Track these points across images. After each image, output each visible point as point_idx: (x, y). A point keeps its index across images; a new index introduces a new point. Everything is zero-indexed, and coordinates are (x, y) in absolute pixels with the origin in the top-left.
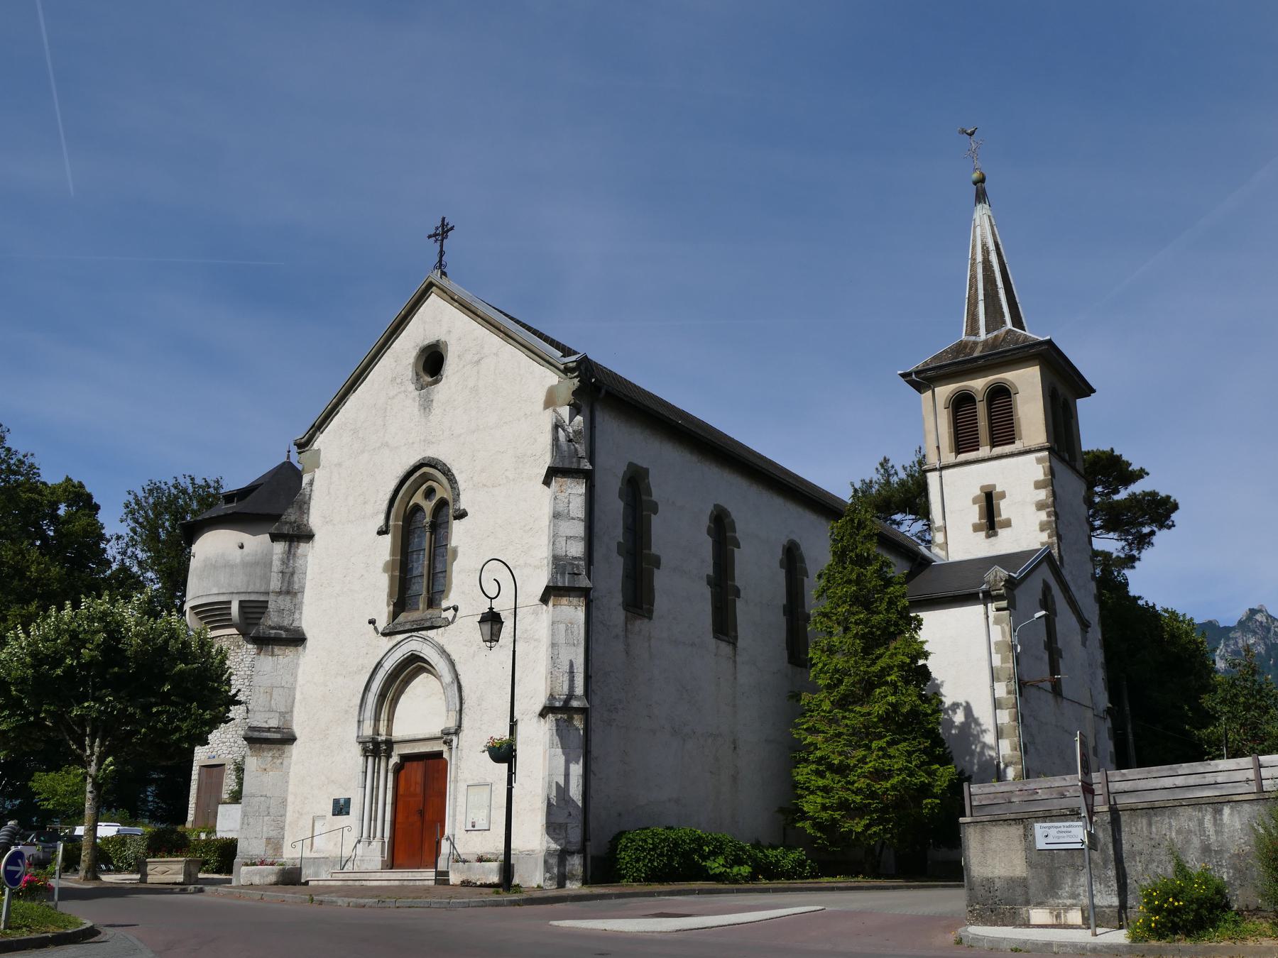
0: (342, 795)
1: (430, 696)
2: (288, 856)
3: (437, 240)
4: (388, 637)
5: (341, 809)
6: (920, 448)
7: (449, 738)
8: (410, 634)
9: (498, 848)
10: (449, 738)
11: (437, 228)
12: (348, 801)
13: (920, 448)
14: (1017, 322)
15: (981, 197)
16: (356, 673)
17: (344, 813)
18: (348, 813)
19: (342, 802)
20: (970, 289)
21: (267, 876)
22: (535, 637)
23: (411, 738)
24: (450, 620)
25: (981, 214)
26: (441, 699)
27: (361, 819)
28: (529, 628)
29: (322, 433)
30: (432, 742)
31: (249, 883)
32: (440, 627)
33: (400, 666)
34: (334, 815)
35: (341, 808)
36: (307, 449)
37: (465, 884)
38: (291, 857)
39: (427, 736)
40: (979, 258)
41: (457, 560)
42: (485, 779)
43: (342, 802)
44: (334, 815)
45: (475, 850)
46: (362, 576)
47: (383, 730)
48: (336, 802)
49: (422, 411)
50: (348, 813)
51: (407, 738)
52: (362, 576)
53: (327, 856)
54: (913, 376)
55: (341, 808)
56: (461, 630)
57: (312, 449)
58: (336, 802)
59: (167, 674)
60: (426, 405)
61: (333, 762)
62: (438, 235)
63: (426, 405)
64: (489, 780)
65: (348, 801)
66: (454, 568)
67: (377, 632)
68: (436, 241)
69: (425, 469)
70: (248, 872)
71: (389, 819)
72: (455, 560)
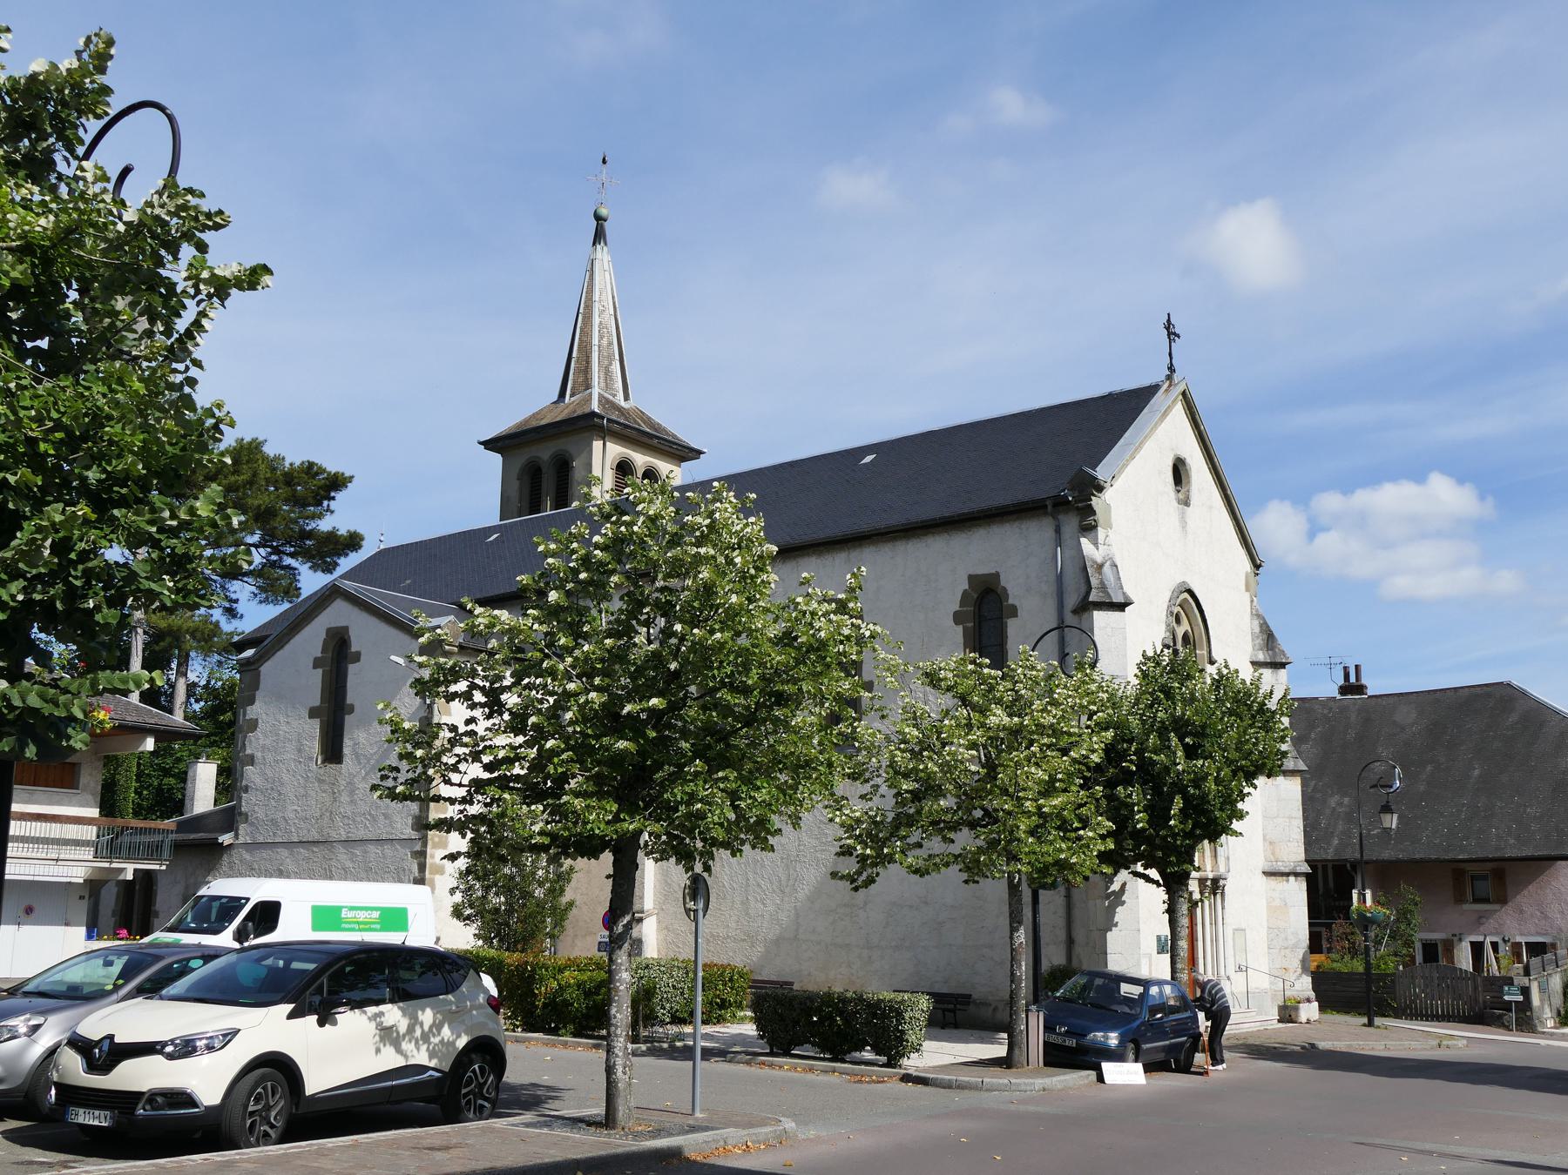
14: (626, 398)
20: (601, 338)
25: (603, 255)
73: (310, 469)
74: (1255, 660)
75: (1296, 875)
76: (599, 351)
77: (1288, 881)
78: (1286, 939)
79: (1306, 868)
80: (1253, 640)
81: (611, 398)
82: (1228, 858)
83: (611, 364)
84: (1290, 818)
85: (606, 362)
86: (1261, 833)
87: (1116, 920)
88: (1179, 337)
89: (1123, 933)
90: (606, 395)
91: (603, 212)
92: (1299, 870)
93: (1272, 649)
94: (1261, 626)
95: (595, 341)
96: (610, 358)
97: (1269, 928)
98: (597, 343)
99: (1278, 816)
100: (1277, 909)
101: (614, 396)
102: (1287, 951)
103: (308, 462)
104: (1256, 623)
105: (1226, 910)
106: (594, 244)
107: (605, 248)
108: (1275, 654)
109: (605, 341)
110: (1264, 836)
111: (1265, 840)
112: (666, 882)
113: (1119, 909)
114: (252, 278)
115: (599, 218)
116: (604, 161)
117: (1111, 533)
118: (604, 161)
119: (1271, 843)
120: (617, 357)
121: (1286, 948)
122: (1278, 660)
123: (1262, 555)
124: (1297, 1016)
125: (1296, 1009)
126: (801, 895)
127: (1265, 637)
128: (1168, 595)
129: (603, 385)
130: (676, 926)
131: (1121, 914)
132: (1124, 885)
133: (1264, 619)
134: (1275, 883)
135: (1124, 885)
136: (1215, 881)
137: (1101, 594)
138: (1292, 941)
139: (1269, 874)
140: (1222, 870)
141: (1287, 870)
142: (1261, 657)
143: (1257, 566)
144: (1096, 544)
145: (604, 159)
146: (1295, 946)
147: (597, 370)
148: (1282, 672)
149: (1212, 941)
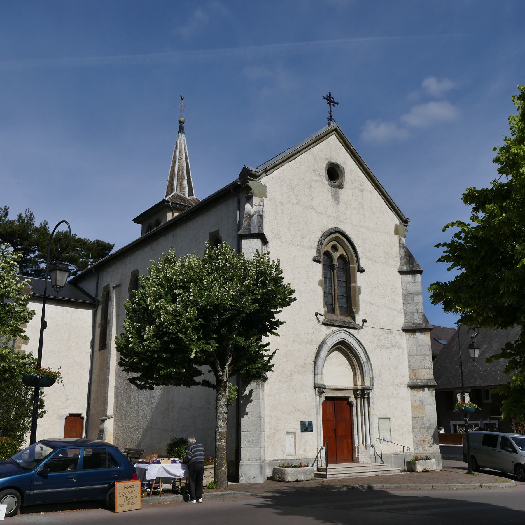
0: (307, 419)
1: (341, 365)
2: (269, 459)
3: (333, 105)
4: (326, 326)
5: (307, 428)
6: (29, 209)
7: (368, 391)
8: (343, 329)
9: (396, 451)
10: (368, 391)
11: (333, 98)
12: (311, 423)
13: (29, 209)
14: (191, 193)
15: (181, 129)
16: (307, 343)
17: (309, 431)
18: (312, 431)
19: (307, 423)
20: (179, 171)
21: (309, 474)
22: (402, 347)
23: (334, 387)
24: (361, 326)
25: (182, 137)
26: (347, 367)
27: (371, 436)
28: (399, 342)
29: (267, 175)
30: (345, 391)
31: (295, 480)
32: (357, 329)
33: (349, 346)
34: (301, 432)
35: (306, 427)
36: (255, 179)
37: (425, 471)
38: (272, 459)
39: (343, 388)
40: (184, 159)
41: (361, 294)
42: (386, 415)
43: (307, 423)
44: (301, 432)
45: (386, 452)
46: (305, 283)
47: (359, 383)
48: (303, 423)
49: (334, 200)
50: (312, 431)
51: (332, 387)
52: (305, 283)
53: (300, 458)
54: (170, 203)
55: (306, 427)
56: (367, 334)
57: (259, 181)
58: (303, 423)
59: (154, 309)
60: (336, 198)
61: (297, 398)
62: (330, 98)
63: (336, 198)
64: (388, 416)
65: (311, 423)
66: (360, 299)
67: (319, 322)
68: (334, 106)
69: (338, 235)
70: (295, 472)
71: (355, 436)
72: (360, 294)
73: (98, 243)
74: (401, 270)
75: (429, 387)
76: (178, 176)
77: (424, 391)
78: (424, 423)
79: (434, 383)
80: (401, 260)
81: (182, 195)
82: (372, 378)
83: (183, 181)
84: (425, 355)
85: (181, 181)
86: (407, 364)
87: (247, 411)
88: (337, 103)
89: (250, 419)
90: (180, 194)
91: (182, 119)
92: (429, 384)
93: (412, 264)
94: (405, 252)
95: (176, 172)
96: (183, 179)
97: (412, 417)
98: (177, 173)
99: (417, 355)
100: (417, 407)
101: (184, 194)
102: (424, 430)
103: (97, 240)
104: (402, 250)
105: (371, 408)
106: (178, 133)
107: (183, 134)
108: (413, 267)
109: (181, 172)
110: (409, 366)
111: (410, 368)
112: (117, 401)
113: (249, 405)
114: (438, 246)
115: (180, 122)
116: (182, 99)
117: (265, 200)
118: (182, 99)
119: (412, 369)
120: (186, 178)
121: (423, 429)
122: (415, 269)
123: (406, 215)
124: (415, 468)
125: (414, 463)
126: (154, 406)
127: (408, 258)
128: (320, 235)
129: (178, 190)
130: (119, 423)
131: (250, 408)
132: (251, 391)
133: (407, 248)
134: (415, 392)
135: (251, 391)
136: (363, 390)
137: (246, 230)
138: (427, 424)
139: (412, 387)
140: (367, 383)
141: (422, 384)
142: (405, 268)
143: (405, 222)
144: (252, 205)
145: (182, 98)
146: (429, 427)
147: (176, 184)
148: (419, 276)
149: (362, 425)
